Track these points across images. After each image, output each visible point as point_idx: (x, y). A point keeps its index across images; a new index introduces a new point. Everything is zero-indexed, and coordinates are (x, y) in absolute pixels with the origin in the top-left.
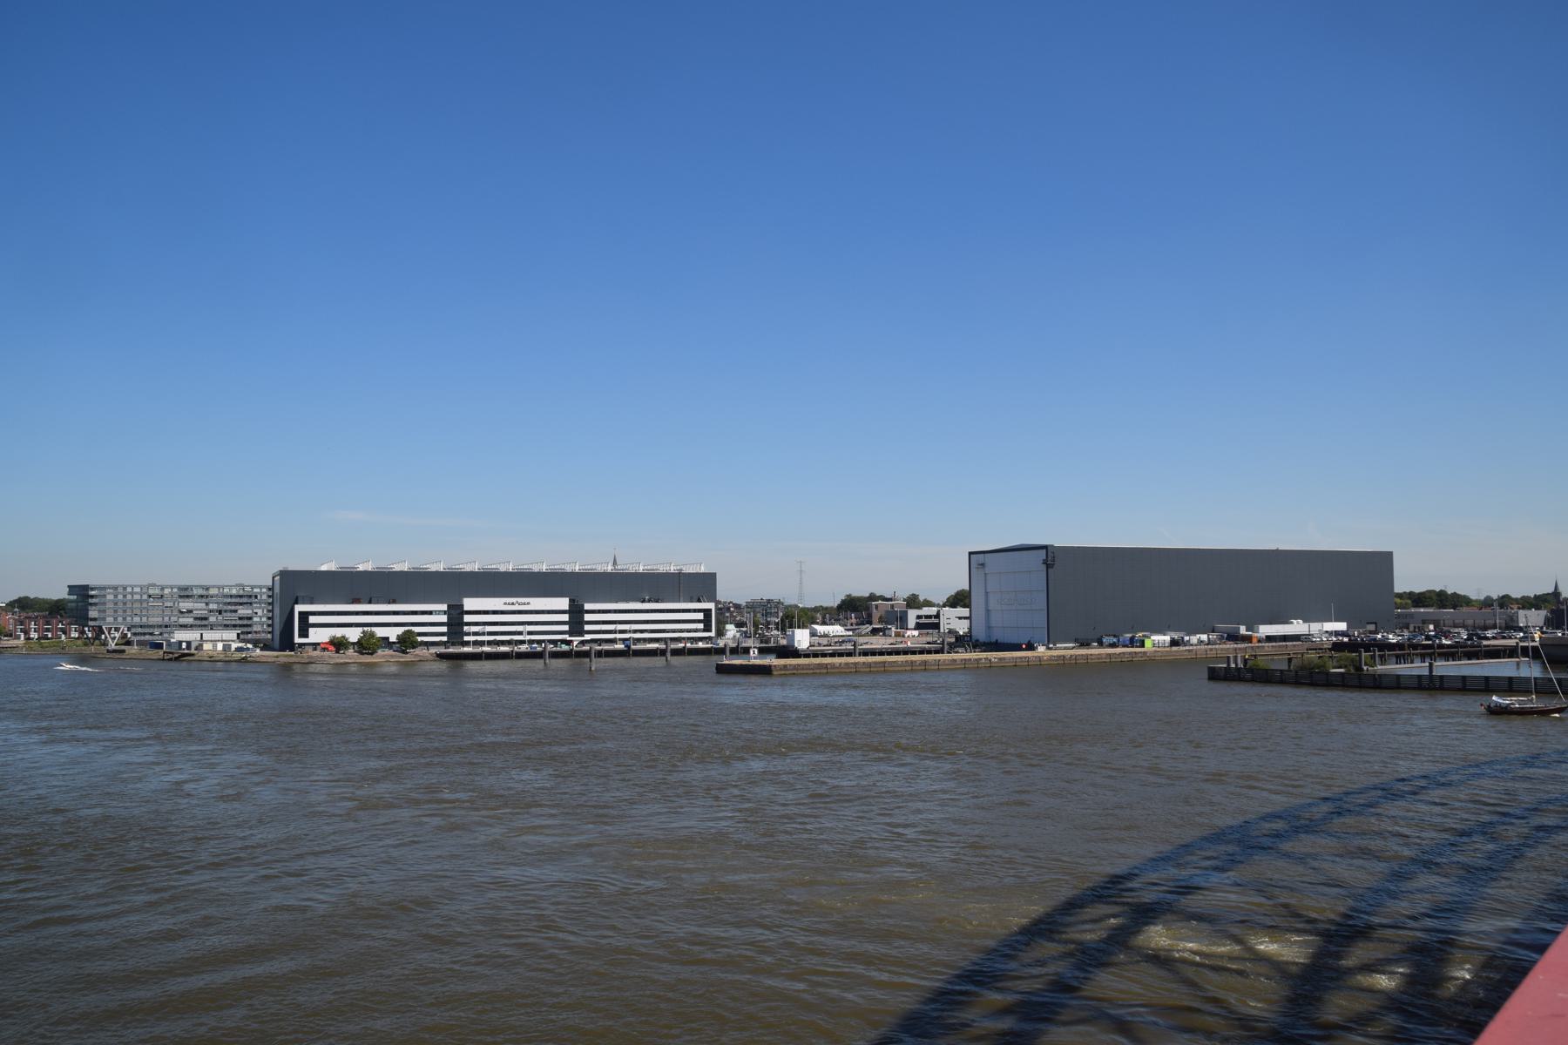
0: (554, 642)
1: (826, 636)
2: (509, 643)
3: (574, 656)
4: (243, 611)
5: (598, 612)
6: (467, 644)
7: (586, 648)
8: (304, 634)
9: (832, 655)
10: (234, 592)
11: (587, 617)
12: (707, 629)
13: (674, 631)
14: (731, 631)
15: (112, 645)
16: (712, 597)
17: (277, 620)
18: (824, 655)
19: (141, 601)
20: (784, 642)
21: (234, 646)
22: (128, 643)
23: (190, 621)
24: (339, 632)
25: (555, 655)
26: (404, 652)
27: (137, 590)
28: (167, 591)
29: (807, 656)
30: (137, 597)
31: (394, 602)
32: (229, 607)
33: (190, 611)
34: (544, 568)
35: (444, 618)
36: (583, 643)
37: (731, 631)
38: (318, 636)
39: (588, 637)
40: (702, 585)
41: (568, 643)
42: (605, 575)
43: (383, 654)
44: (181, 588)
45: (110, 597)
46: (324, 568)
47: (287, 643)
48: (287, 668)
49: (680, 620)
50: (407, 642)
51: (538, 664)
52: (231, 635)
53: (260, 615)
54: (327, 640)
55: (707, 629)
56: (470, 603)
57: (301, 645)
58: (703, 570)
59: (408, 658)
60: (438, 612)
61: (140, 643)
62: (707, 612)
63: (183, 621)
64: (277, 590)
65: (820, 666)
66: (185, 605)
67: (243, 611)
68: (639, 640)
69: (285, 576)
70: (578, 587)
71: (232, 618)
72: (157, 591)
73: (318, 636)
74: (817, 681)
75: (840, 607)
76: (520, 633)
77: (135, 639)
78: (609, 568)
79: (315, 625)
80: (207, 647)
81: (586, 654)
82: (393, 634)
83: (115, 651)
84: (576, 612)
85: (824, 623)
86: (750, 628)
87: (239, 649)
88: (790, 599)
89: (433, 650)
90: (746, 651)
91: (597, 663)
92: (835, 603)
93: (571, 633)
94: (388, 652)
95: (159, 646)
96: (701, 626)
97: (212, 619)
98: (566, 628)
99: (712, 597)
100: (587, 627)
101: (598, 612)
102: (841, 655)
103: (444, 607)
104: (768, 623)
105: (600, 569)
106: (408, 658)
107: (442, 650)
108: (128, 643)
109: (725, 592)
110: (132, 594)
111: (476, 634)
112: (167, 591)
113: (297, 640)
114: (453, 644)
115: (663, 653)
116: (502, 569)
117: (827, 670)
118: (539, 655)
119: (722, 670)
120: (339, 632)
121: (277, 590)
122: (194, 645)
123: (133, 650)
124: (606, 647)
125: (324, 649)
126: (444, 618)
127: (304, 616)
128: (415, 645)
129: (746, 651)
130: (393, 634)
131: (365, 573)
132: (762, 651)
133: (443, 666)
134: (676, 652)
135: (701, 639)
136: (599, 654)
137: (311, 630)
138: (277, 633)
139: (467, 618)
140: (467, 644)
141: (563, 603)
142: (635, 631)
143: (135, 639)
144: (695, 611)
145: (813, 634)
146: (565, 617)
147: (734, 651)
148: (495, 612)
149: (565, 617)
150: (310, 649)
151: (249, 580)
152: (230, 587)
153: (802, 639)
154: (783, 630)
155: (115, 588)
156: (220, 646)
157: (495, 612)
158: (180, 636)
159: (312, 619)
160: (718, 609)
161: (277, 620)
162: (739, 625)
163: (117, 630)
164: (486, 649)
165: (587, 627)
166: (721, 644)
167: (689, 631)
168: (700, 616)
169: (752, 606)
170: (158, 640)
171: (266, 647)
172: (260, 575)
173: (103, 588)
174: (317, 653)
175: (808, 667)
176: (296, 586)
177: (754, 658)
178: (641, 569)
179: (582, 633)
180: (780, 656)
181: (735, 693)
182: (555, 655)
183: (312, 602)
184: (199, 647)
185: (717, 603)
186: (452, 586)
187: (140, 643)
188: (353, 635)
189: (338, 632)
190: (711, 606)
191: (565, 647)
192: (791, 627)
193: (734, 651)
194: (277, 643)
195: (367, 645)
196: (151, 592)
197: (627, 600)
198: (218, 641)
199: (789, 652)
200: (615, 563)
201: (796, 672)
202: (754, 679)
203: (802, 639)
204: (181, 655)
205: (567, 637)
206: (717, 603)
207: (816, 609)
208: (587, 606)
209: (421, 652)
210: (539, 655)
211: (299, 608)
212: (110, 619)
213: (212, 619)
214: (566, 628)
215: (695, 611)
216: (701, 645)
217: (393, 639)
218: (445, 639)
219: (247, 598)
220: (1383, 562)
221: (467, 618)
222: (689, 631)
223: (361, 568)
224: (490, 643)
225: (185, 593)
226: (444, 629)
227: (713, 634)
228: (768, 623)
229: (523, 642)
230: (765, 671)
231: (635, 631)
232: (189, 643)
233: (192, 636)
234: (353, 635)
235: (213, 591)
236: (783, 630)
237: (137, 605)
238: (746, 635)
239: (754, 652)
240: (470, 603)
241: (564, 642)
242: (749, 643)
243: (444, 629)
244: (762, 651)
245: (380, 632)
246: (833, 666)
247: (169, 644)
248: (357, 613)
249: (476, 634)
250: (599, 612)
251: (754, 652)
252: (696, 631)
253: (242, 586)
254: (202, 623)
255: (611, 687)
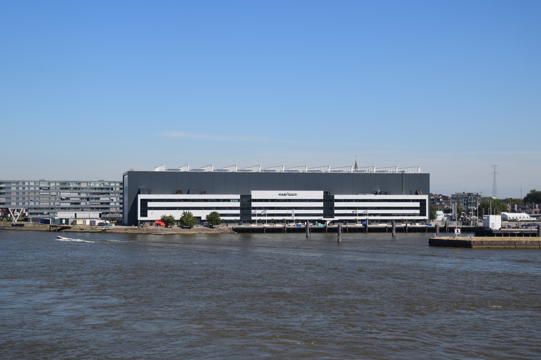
0: (313, 221)
1: (514, 220)
2: (282, 221)
3: (328, 231)
4: (103, 199)
5: (344, 200)
6: (254, 222)
7: (336, 226)
8: (144, 214)
9: (520, 235)
10: (97, 185)
11: (336, 204)
12: (423, 213)
13: (398, 215)
14: (440, 215)
15: (15, 221)
16: (426, 191)
17: (126, 204)
18: (513, 235)
19: (35, 192)
20: (481, 224)
21: (97, 222)
22: (26, 220)
23: (68, 205)
24: (168, 213)
25: (314, 230)
26: (211, 227)
27: (32, 184)
28: (52, 185)
29: (499, 235)
30: (32, 189)
31: (204, 193)
32: (94, 196)
33: (68, 199)
34: (306, 170)
35: (238, 204)
36: (333, 222)
37: (440, 215)
38: (152, 215)
39: (337, 218)
40: (418, 182)
41: (323, 222)
42: (349, 175)
43: (197, 228)
44: (61, 183)
45: (14, 189)
46: (157, 170)
47: (133, 221)
48: (132, 236)
49: (403, 207)
50: (213, 220)
51: (302, 236)
52: (95, 214)
53: (115, 201)
54: (159, 218)
55: (423, 213)
56: (255, 194)
57: (142, 222)
58: (420, 171)
59: (213, 231)
60: (233, 200)
61: (34, 220)
62: (422, 202)
63: (63, 205)
64: (126, 184)
65: (510, 243)
66: (64, 194)
67: (103, 199)
68: (373, 221)
69: (132, 175)
70: (330, 184)
71: (95, 203)
72: (46, 185)
73: (152, 215)
74: (509, 255)
75: (526, 199)
76: (290, 215)
77: (31, 217)
78: (352, 170)
79: (151, 208)
80: (79, 222)
81: (335, 230)
82: (204, 215)
83: (17, 225)
84: (329, 201)
85: (513, 211)
86: (454, 213)
87: (100, 224)
88: (486, 193)
89: (231, 226)
90: (452, 230)
91: (343, 237)
92: (522, 196)
93: (325, 215)
94: (200, 227)
95: (47, 222)
96: (418, 212)
97: (83, 204)
98: (321, 212)
99: (426, 191)
100: (336, 212)
101: (344, 200)
102: (527, 235)
103: (238, 197)
104: (469, 210)
105: (345, 170)
106: (213, 231)
107: (237, 226)
108: (26, 220)
109: (436, 187)
110: (29, 186)
111: (259, 215)
112: (52, 185)
113: (140, 218)
114: (244, 222)
115: (390, 230)
116: (278, 170)
117: (516, 246)
118: (303, 230)
119: (433, 243)
120: (168, 213)
121: (126, 184)
122: (70, 221)
123: (29, 224)
124: (350, 225)
125: (158, 225)
126: (238, 204)
127: (144, 202)
128: (218, 222)
129: (452, 230)
130: (204, 215)
131: (185, 173)
132: (464, 231)
133: (236, 237)
134: (399, 230)
135: (418, 221)
136: (345, 230)
137: (322, 197)
138: (126, 213)
139: (254, 204)
140: (254, 222)
141: (319, 194)
142: (370, 215)
143: (31, 217)
144: (414, 201)
145: (504, 219)
146: (321, 204)
147: (443, 230)
148: (273, 200)
149: (321, 204)
150: (148, 224)
151: (108, 177)
152: (95, 182)
153: (495, 222)
154: (480, 216)
155: (17, 183)
156: (88, 222)
157: (273, 200)
158: (61, 215)
159: (150, 204)
160: (430, 200)
161: (126, 204)
162: (447, 211)
163: (18, 211)
164: (267, 225)
165: (336, 212)
166: (433, 224)
167: (409, 215)
168: (418, 204)
169: (456, 198)
170: (46, 217)
171: (119, 222)
172: (115, 175)
173: (10, 183)
174: (153, 227)
175: (497, 243)
176: (139, 182)
177: (458, 236)
178: (375, 171)
179: (332, 215)
180: (477, 235)
181: (447, 261)
182: (314, 230)
183: (149, 193)
184: (74, 223)
185: (430, 195)
186: (243, 182)
187: (34, 220)
188: (177, 215)
189: (167, 213)
190: (425, 197)
191: (320, 225)
192: (486, 213)
193: (443, 230)
194: (126, 220)
195: (186, 222)
196: (41, 185)
197: (364, 193)
198: (87, 218)
199: (486, 231)
200: (356, 167)
201: (490, 246)
202: (458, 251)
203: (495, 222)
204: (63, 228)
205: (322, 218)
206: (430, 195)
207: (506, 201)
208: (336, 197)
209: (222, 227)
210: (303, 230)
211: (141, 197)
212: (14, 204)
213: (83, 204)
214: (321, 212)
215: (414, 201)
216: (417, 225)
217: (204, 218)
218: (238, 218)
219: (106, 190)
220: (200, 217)
221: (254, 204)
222: (409, 215)
223: (182, 170)
224: (269, 222)
225: (64, 186)
226: (238, 212)
227: (427, 217)
228: (469, 210)
229: (291, 221)
230: (467, 245)
231: (370, 215)
232: (67, 220)
233: (69, 215)
234: (177, 215)
235: (83, 185)
236: (480, 216)
237: (32, 194)
238: (452, 219)
239: (457, 231)
240: (255, 194)
241: (320, 221)
242: (454, 224)
243: (238, 212)
244: (464, 231)
245: (195, 213)
246: (520, 243)
247: (54, 220)
248: (180, 200)
249: (259, 215)
250: (345, 201)
251: (457, 231)
252: (414, 215)
253: (103, 182)
254: (76, 206)
255: (352, 254)
